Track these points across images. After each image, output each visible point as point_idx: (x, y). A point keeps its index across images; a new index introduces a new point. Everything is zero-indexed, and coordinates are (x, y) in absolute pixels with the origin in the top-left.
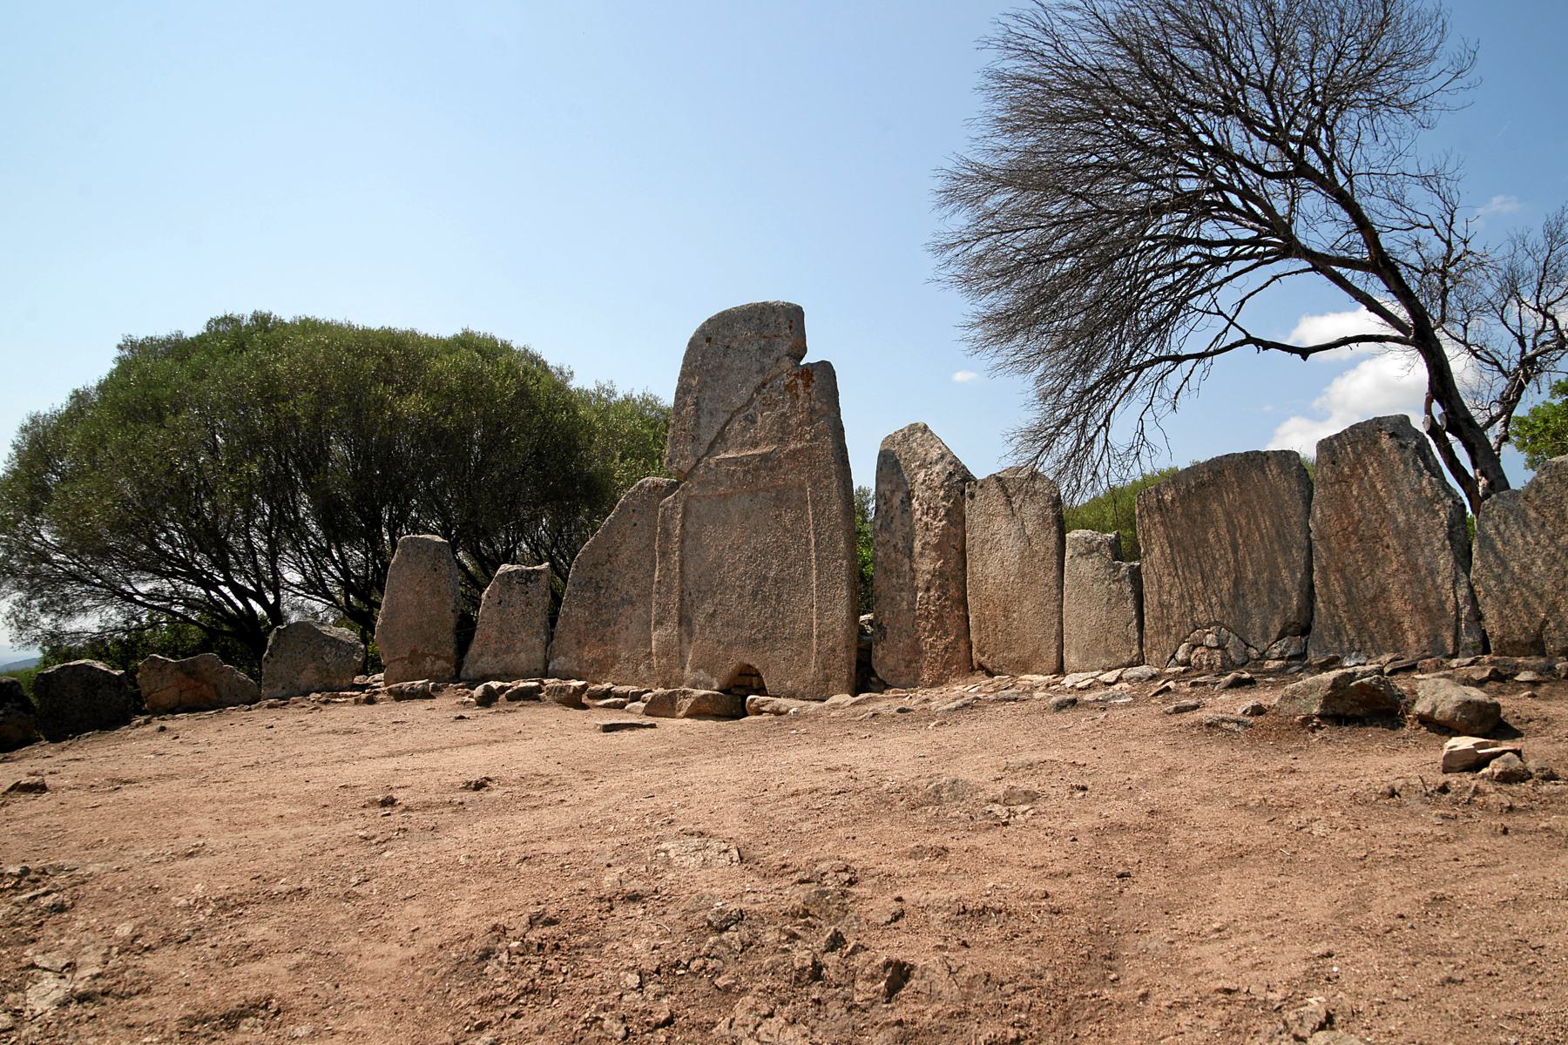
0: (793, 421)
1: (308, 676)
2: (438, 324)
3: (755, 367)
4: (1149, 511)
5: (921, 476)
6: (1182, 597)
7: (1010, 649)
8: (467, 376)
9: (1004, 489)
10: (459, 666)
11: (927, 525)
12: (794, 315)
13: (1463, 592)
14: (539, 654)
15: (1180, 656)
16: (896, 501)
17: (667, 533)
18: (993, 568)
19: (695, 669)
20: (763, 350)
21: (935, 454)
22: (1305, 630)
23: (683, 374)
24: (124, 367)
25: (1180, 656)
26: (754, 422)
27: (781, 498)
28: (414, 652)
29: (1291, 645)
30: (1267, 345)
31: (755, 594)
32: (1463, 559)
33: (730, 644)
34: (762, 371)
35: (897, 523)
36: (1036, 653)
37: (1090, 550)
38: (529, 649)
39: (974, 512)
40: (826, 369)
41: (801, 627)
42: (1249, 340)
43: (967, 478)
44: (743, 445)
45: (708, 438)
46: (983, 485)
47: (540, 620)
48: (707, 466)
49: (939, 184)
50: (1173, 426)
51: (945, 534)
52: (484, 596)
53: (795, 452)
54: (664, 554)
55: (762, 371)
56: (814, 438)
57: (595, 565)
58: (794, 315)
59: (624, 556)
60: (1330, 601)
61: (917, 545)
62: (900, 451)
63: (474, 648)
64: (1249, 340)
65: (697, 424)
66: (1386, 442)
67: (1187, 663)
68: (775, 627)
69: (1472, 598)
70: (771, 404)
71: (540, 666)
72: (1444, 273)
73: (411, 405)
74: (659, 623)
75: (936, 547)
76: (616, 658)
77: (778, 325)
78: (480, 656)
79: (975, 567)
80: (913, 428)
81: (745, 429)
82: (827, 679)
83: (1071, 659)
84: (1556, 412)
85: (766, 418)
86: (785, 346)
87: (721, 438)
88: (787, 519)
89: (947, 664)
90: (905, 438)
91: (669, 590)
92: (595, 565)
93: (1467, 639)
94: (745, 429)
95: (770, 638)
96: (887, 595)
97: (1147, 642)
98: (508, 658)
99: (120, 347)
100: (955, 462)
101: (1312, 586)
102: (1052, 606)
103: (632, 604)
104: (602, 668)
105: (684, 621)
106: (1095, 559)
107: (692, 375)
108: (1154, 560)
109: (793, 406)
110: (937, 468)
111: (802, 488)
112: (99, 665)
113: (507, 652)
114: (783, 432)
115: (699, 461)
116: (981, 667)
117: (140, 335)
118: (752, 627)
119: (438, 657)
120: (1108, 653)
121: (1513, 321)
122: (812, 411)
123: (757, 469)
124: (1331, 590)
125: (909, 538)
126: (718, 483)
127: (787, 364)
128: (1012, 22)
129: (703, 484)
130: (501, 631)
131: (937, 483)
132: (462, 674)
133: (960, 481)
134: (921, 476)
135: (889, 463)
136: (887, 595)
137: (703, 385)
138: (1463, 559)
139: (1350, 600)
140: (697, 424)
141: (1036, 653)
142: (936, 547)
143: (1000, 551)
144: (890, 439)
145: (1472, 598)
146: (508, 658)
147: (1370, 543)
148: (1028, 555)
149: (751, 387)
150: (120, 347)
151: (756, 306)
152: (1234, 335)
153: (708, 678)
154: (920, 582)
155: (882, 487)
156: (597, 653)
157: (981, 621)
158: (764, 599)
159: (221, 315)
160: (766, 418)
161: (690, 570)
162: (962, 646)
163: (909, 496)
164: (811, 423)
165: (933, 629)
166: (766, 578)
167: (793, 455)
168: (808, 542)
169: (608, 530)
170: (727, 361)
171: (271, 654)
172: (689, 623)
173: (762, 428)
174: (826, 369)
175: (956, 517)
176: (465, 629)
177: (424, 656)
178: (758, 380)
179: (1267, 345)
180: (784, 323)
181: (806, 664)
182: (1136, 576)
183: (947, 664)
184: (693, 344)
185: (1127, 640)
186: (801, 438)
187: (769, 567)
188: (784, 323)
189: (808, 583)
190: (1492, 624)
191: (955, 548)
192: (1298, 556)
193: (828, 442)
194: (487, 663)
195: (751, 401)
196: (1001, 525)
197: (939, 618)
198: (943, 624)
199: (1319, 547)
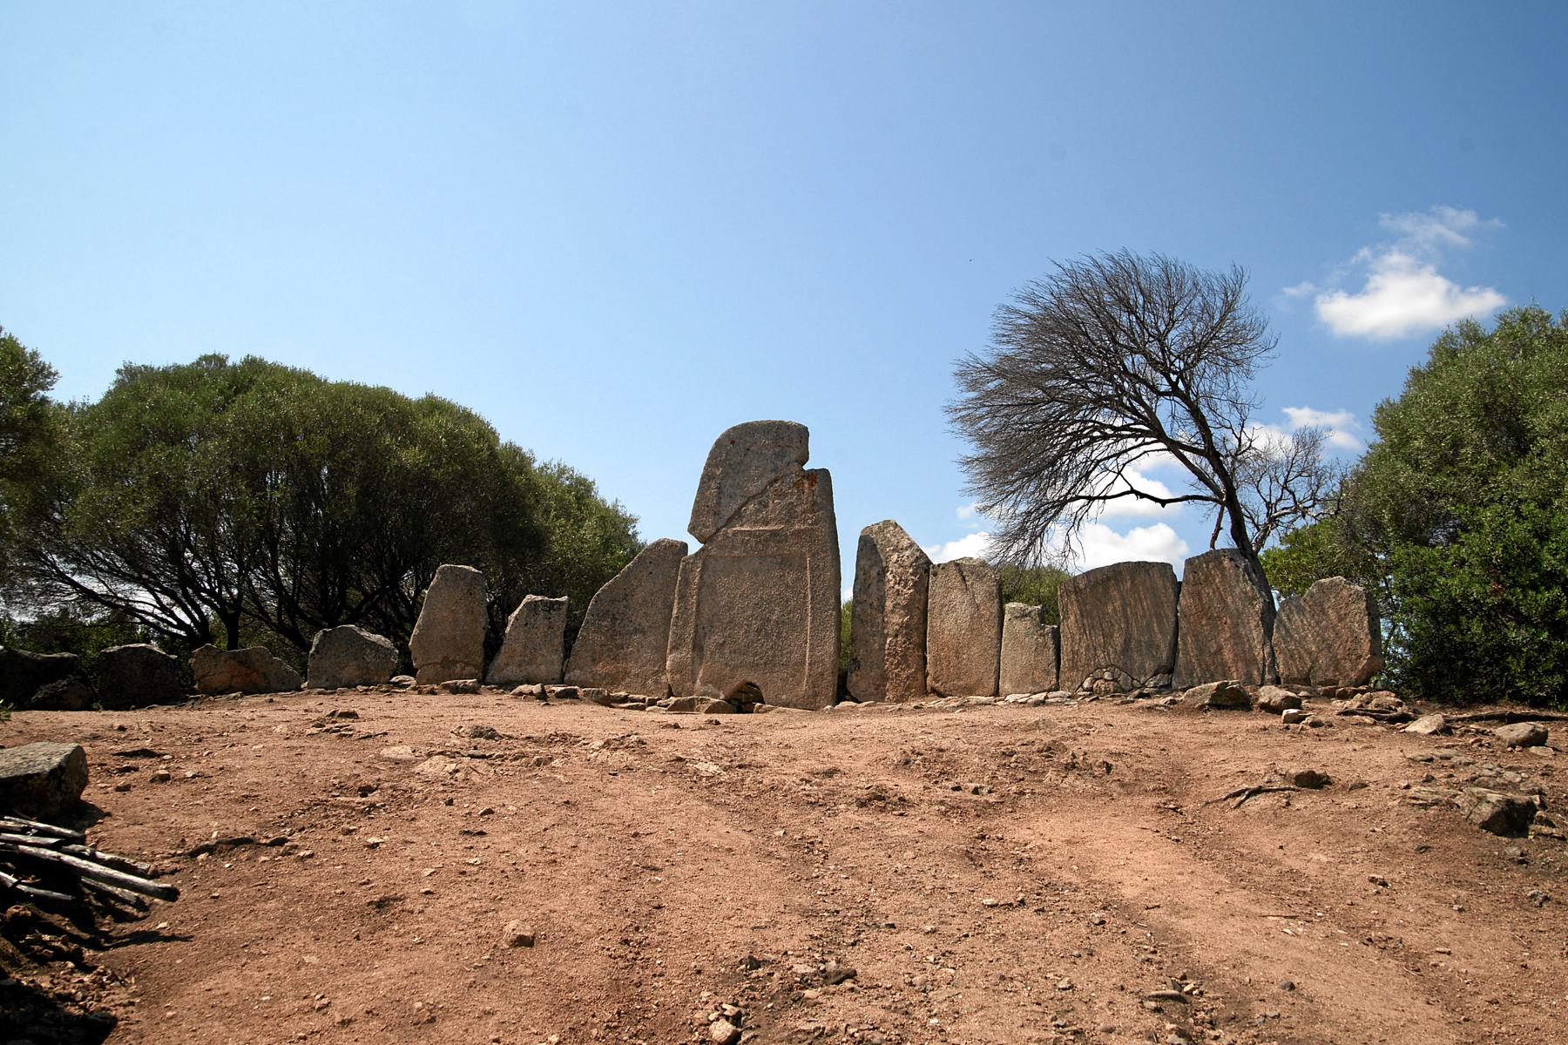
0: (799, 509)
1: (349, 672)
2: (412, 390)
3: (770, 467)
4: (1068, 593)
5: (895, 557)
6: (1087, 649)
7: (959, 679)
8: (451, 436)
9: (961, 572)
10: (485, 672)
11: (897, 591)
12: (803, 433)
13: (1267, 650)
14: (557, 668)
15: (1086, 685)
16: (874, 573)
17: (686, 582)
18: (949, 624)
19: (704, 683)
20: (777, 455)
21: (905, 543)
22: (1171, 671)
23: (708, 465)
24: (120, 384)
25: (1086, 685)
26: (766, 506)
27: (785, 562)
28: (446, 659)
29: (1161, 679)
30: (1143, 496)
31: (759, 631)
32: (1268, 633)
33: (736, 667)
34: (775, 470)
35: (873, 588)
36: (979, 682)
37: (1024, 615)
38: (550, 660)
39: (936, 585)
40: (824, 475)
41: (795, 657)
42: (1132, 491)
43: (929, 562)
44: (756, 522)
45: (727, 514)
46: (944, 567)
47: (558, 641)
48: (726, 534)
49: (956, 369)
50: (1091, 543)
51: (912, 599)
52: (512, 617)
53: (799, 532)
54: (682, 597)
55: (775, 470)
56: (816, 523)
57: (613, 601)
58: (803, 433)
59: (640, 595)
60: (1186, 654)
61: (889, 604)
62: (879, 539)
63: (501, 659)
64: (1132, 491)
65: (719, 503)
66: (1226, 563)
67: (1091, 689)
68: (774, 656)
69: (1272, 654)
70: (781, 495)
71: (557, 676)
72: (1235, 457)
73: (411, 456)
74: (675, 648)
75: (904, 607)
76: (627, 673)
77: (791, 439)
78: (504, 663)
79: (933, 623)
80: (887, 523)
81: (758, 511)
82: (816, 695)
83: (1005, 686)
84: (1282, 555)
85: (775, 505)
86: (794, 455)
87: (737, 516)
88: (790, 578)
89: (908, 688)
90: (881, 530)
91: (686, 623)
92: (613, 601)
93: (1267, 677)
94: (758, 511)
95: (770, 664)
96: (880, 639)
97: (1062, 677)
98: (531, 669)
99: (119, 372)
100: (919, 550)
101: (1176, 644)
102: (993, 652)
103: (644, 633)
104: (614, 681)
105: (698, 647)
106: (1027, 622)
107: (717, 466)
108: (1070, 624)
109: (799, 499)
110: (907, 553)
111: (803, 557)
112: (66, 655)
113: (529, 664)
114: (790, 515)
115: (718, 530)
116: (934, 691)
117: (139, 361)
118: (756, 654)
119: (467, 664)
120: (1034, 683)
121: (1265, 491)
122: (814, 504)
123: (767, 540)
124: (1187, 644)
125: (882, 600)
126: (734, 548)
127: (795, 467)
128: (1032, 285)
129: (722, 547)
130: (525, 647)
131: (907, 563)
132: (488, 679)
133: (924, 567)
134: (895, 557)
135: (868, 546)
136: (880, 639)
137: (725, 475)
138: (1268, 633)
139: (1201, 652)
140: (719, 503)
141: (979, 682)
142: (904, 607)
143: (952, 616)
144: (870, 528)
145: (1272, 654)
146: (531, 669)
147: (1214, 621)
148: (976, 617)
149: (765, 481)
150: (119, 372)
151: (774, 423)
152: (1120, 486)
153: (716, 691)
154: (890, 630)
155: (862, 562)
156: (610, 668)
157: (937, 660)
158: (767, 635)
159: (210, 353)
160: (775, 505)
161: (706, 609)
162: (920, 676)
163: (884, 571)
164: (813, 512)
165: (899, 664)
166: (769, 620)
167: (798, 533)
168: (806, 596)
169: (626, 575)
170: (747, 460)
171: (317, 651)
172: (701, 649)
173: (773, 511)
174: (824, 475)
175: (922, 588)
176: (493, 643)
177: (455, 662)
178: (773, 476)
179: (1143, 496)
180: (792, 439)
181: (799, 683)
182: (1056, 635)
183: (908, 688)
184: (718, 443)
185: (1048, 673)
186: (805, 521)
187: (772, 612)
188: (792, 439)
189: (803, 630)
190: (1281, 669)
191: (919, 608)
192: (1169, 627)
193: (823, 529)
194: (512, 672)
195: (764, 491)
196: (957, 596)
197: (904, 656)
198: (906, 661)
199: (1182, 624)
